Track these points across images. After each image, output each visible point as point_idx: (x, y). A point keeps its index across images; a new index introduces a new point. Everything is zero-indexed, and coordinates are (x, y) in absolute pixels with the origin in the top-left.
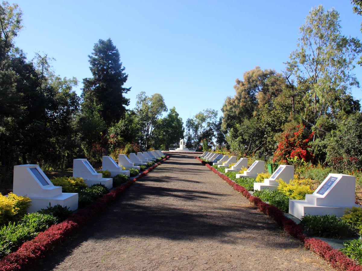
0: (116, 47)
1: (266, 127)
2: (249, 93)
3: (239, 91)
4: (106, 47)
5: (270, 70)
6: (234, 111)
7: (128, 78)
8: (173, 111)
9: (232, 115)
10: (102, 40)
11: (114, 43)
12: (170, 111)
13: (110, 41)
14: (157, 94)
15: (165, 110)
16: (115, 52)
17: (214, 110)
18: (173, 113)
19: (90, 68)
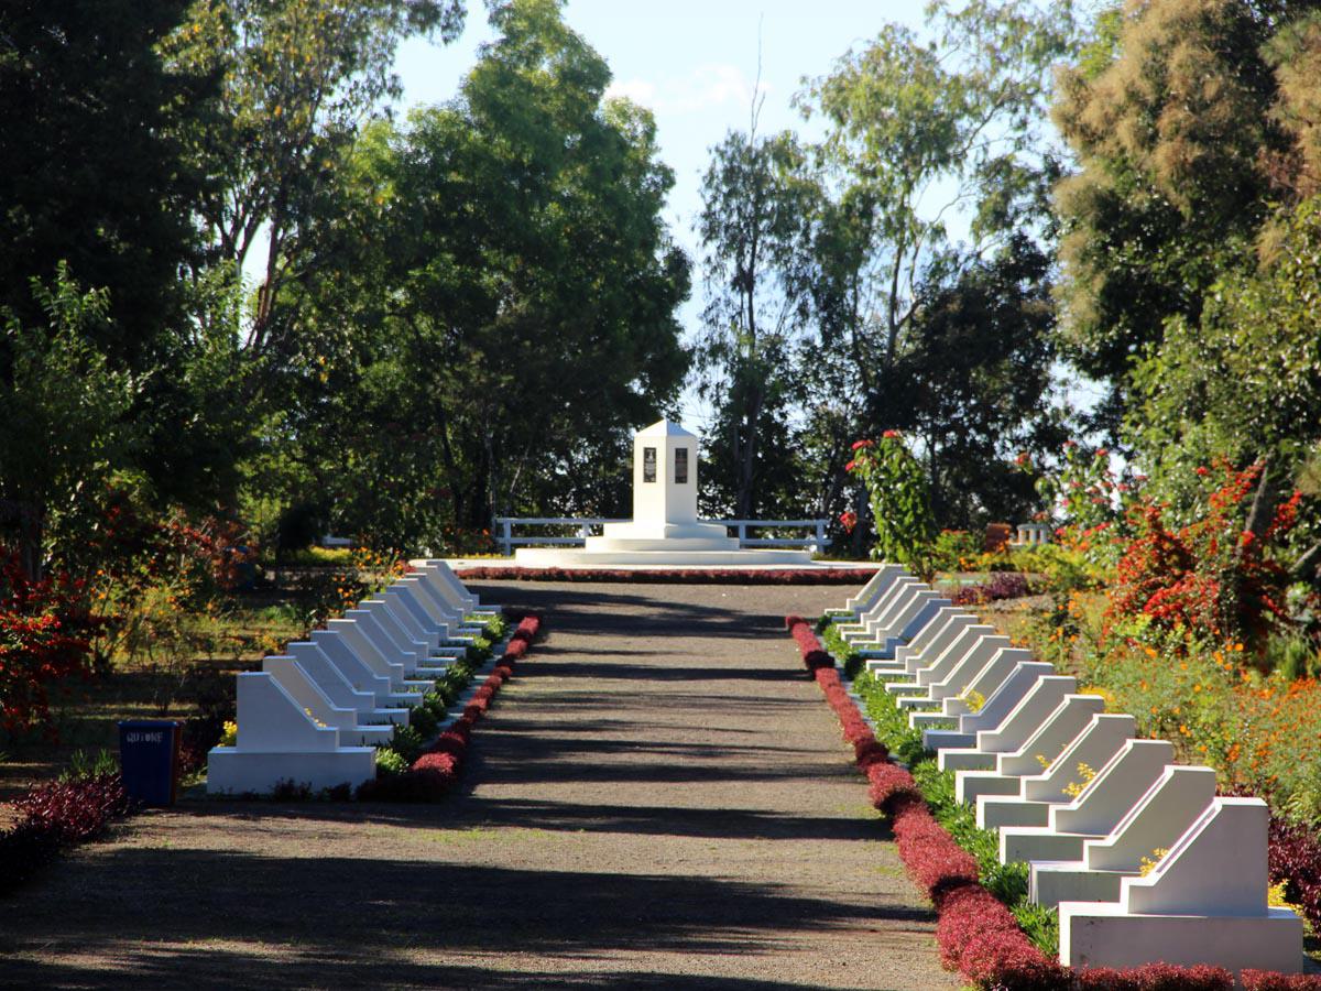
12: (495, 35)
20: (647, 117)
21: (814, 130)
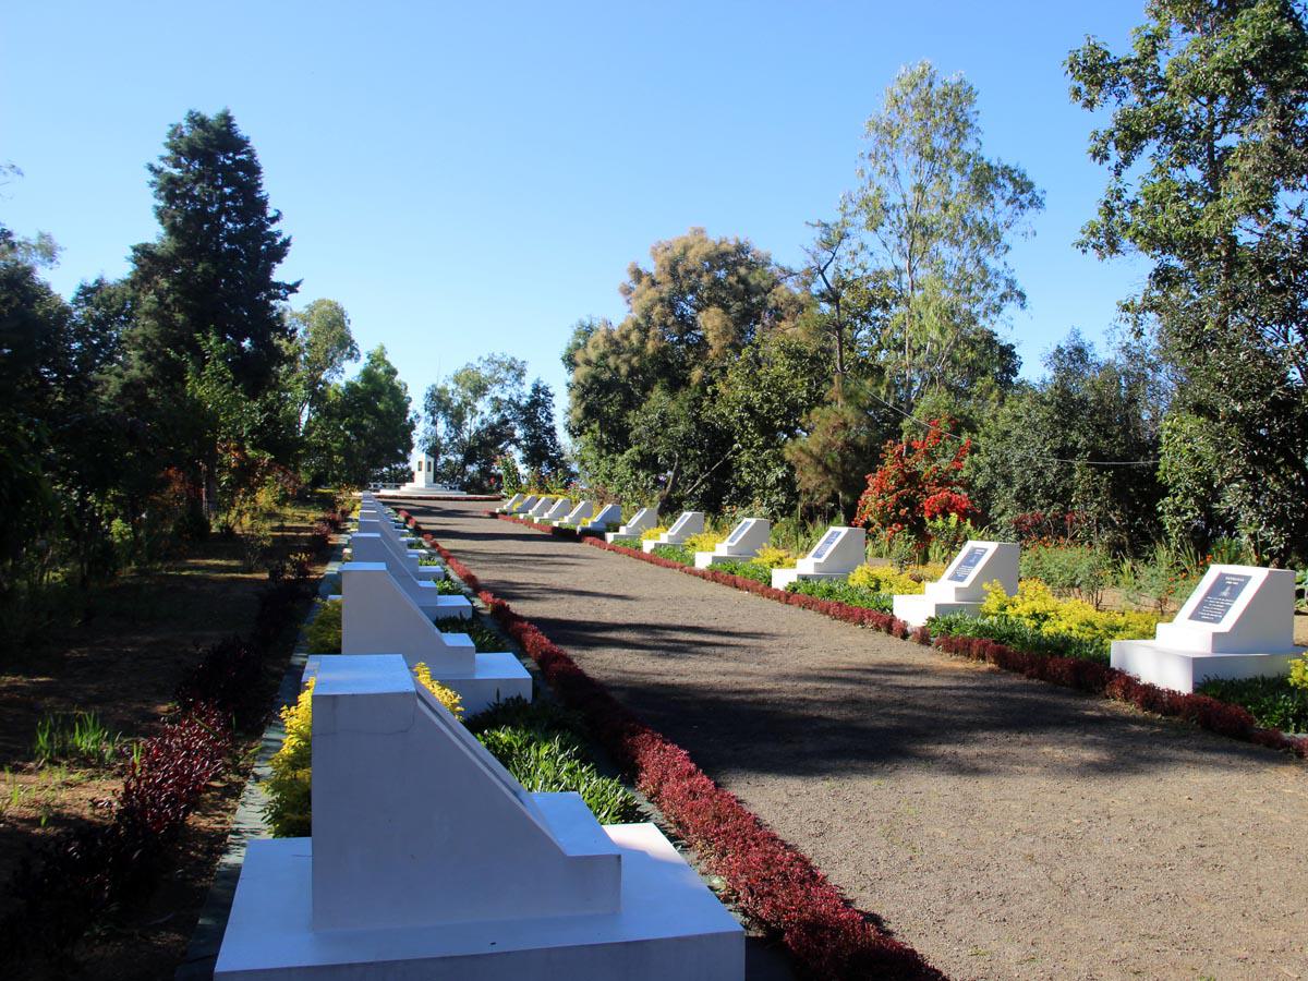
0: (248, 142)
1: (741, 419)
2: (672, 306)
3: (645, 301)
4: (214, 137)
5: (737, 240)
6: (612, 365)
7: (291, 250)
8: (378, 359)
9: (606, 376)
10: (198, 114)
11: (243, 128)
12: (368, 361)
13: (227, 119)
14: (324, 300)
15: (351, 356)
16: (244, 157)
17: (513, 359)
18: (379, 365)
19: (158, 208)
20: (405, 385)
21: (451, 386)
